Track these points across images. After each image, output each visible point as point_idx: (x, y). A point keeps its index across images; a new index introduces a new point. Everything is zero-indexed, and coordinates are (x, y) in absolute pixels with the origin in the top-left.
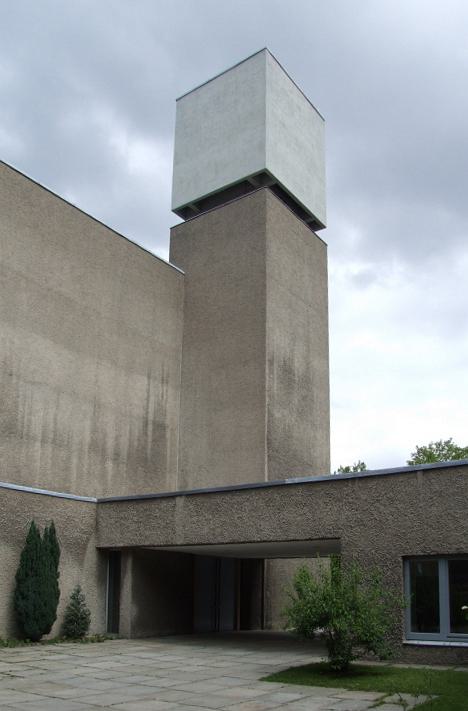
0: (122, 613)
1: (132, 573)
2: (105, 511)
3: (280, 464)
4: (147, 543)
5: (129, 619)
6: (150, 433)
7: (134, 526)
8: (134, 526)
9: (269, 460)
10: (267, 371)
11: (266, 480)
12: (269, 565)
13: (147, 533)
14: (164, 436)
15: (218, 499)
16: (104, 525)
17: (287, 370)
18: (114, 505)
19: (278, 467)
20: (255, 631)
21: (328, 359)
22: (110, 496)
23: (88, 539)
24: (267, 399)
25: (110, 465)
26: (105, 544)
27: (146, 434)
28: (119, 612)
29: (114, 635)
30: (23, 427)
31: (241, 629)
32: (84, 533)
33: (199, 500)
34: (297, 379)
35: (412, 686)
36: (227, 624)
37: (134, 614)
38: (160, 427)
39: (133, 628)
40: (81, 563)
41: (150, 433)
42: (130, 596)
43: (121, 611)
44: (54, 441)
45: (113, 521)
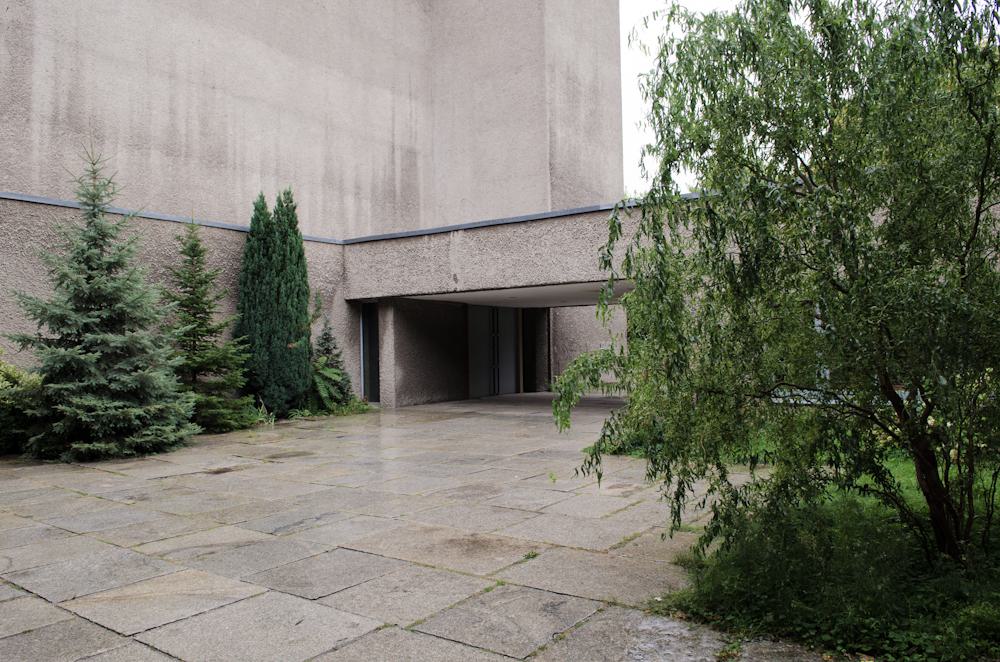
0: (382, 377)
1: (395, 328)
2: (352, 254)
3: (565, 193)
4: (414, 291)
5: (393, 384)
6: (398, 161)
7: (396, 271)
8: (396, 271)
9: (553, 189)
10: (548, 79)
11: (550, 211)
12: (555, 314)
13: (414, 279)
14: (415, 165)
15: (509, 232)
16: (354, 272)
17: (571, 78)
18: (366, 247)
19: (563, 197)
20: (538, 394)
21: (619, 66)
22: (353, 236)
23: (334, 290)
24: (548, 114)
25: (350, 201)
26: (353, 296)
27: (393, 162)
28: (379, 376)
29: (373, 406)
30: (234, 154)
31: (525, 391)
32: (330, 282)
33: (482, 234)
34: (583, 89)
35: (238, 309)
36: (508, 380)
37: (399, 378)
38: (411, 154)
39: (398, 396)
40: (41, 376)
41: (398, 161)
42: (392, 356)
43: (381, 375)
44: (277, 172)
45: (366, 266)
